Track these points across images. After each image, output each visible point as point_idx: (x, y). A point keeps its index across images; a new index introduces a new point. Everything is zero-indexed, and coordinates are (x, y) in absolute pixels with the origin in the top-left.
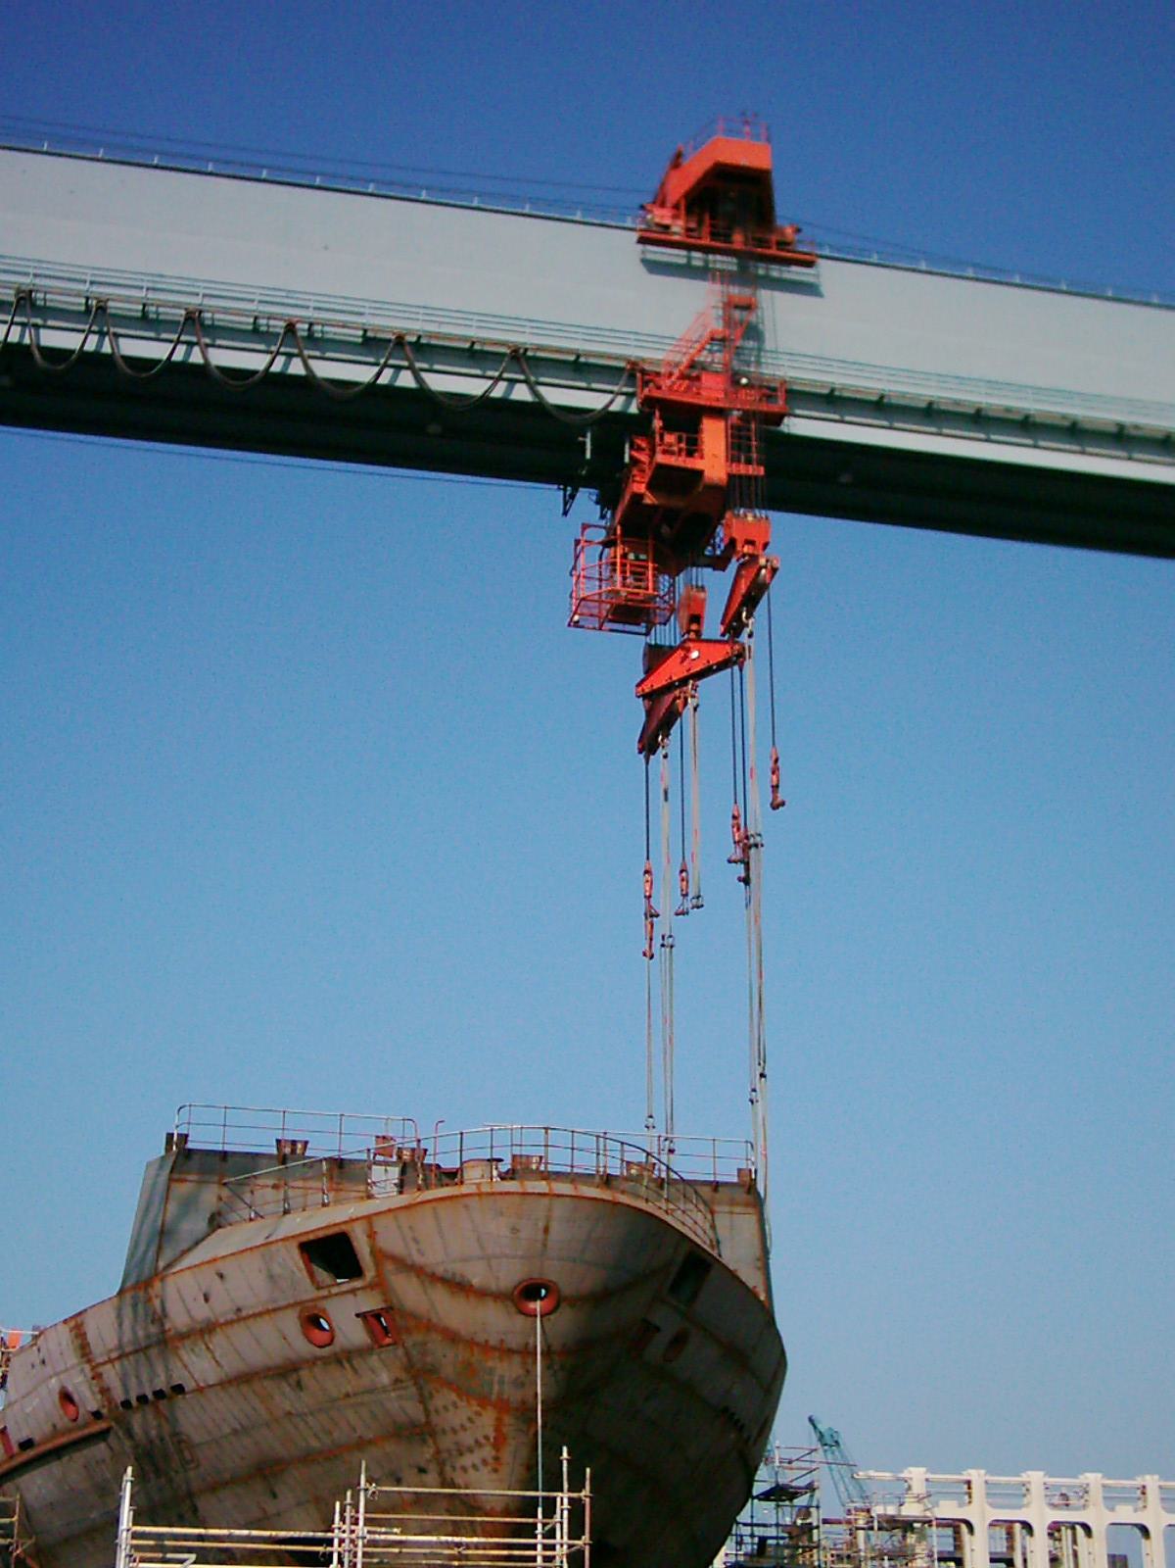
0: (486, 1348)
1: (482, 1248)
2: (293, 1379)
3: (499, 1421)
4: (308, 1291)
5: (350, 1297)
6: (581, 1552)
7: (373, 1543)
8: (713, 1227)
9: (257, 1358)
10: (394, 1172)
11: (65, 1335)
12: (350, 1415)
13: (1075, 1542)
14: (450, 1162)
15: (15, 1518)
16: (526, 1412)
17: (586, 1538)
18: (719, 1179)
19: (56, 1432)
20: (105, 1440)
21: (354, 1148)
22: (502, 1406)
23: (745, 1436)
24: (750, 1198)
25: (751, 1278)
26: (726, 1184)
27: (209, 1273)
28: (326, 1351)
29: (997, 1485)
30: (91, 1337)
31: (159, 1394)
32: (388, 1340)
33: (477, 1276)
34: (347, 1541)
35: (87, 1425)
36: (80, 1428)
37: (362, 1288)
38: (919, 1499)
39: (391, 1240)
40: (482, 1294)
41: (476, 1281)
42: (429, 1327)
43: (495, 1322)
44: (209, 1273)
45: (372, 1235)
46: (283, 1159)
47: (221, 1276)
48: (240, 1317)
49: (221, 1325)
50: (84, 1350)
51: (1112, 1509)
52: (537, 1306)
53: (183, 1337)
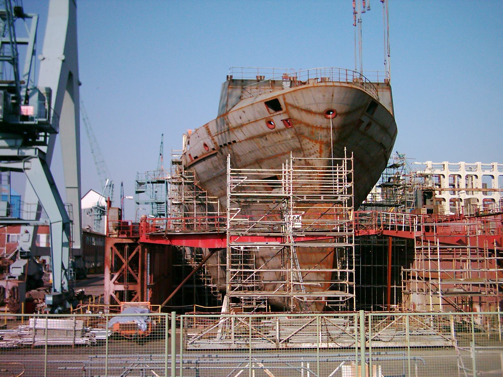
0: (317, 128)
1: (315, 101)
2: (265, 138)
3: (321, 147)
4: (268, 115)
5: (279, 116)
6: (351, 174)
7: (294, 172)
8: (377, 95)
9: (255, 133)
10: (289, 83)
11: (204, 130)
12: (280, 146)
13: (472, 180)
14: (303, 80)
15: (194, 176)
16: (328, 144)
17: (352, 170)
18: (379, 82)
19: (203, 154)
20: (216, 156)
21: (278, 77)
22: (321, 143)
23: (386, 150)
24: (388, 87)
25: (389, 109)
26: (381, 83)
27: (241, 111)
28: (273, 130)
29: (452, 165)
30: (210, 130)
31: (230, 143)
32: (290, 127)
33: (314, 108)
34: (287, 172)
35: (211, 152)
36: (209, 153)
37: (283, 113)
38: (430, 169)
39: (290, 100)
40: (315, 113)
41: (313, 110)
42: (301, 122)
43: (319, 121)
44: (241, 111)
45: (284, 99)
46: (258, 81)
47: (244, 112)
48: (250, 122)
49: (245, 125)
50: (209, 133)
51: (484, 171)
52: (330, 116)
53: (235, 128)
